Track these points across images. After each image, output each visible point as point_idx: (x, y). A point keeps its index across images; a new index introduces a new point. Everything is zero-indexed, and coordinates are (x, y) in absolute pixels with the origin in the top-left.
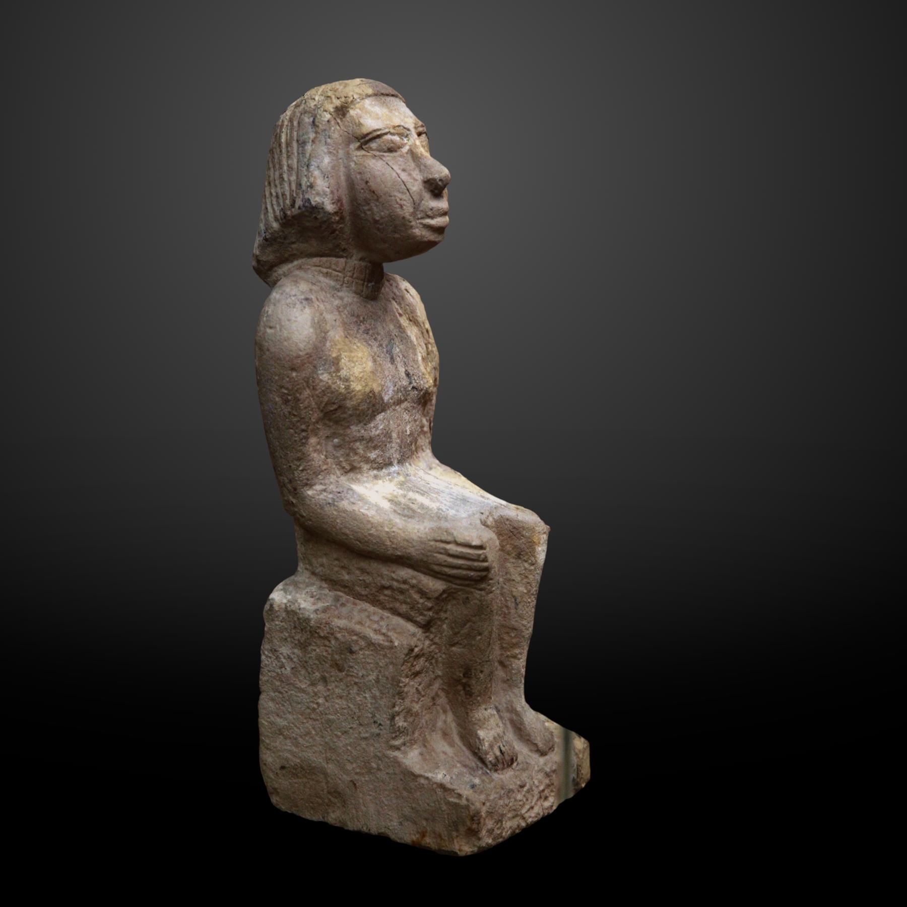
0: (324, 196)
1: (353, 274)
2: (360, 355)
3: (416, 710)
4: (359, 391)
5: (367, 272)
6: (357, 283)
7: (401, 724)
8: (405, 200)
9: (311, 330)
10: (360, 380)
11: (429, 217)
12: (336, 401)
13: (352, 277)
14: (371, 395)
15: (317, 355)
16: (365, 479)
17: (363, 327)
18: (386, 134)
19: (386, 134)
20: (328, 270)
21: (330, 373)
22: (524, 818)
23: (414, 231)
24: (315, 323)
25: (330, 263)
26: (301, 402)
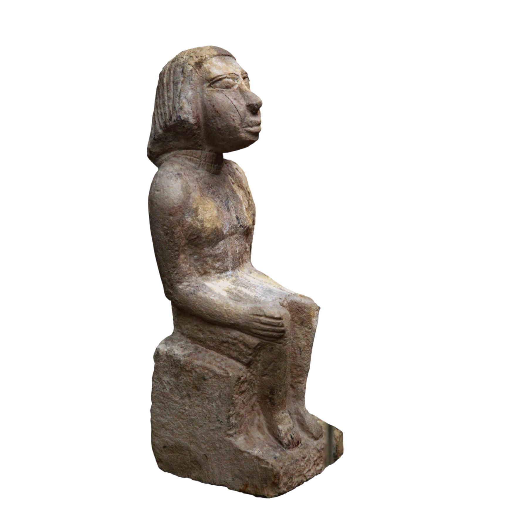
0: (189, 114)
1: (206, 159)
2: (210, 207)
3: (242, 413)
4: (209, 228)
5: (214, 158)
6: (208, 165)
7: (233, 421)
8: (236, 117)
9: (181, 192)
10: (210, 221)
11: (250, 126)
12: (196, 234)
13: (205, 161)
14: (216, 230)
15: (184, 207)
16: (213, 279)
17: (211, 190)
18: (225, 78)
19: (225, 78)
20: (191, 157)
21: (192, 217)
23: (241, 134)
24: (183, 188)
25: (192, 153)
26: (175, 234)
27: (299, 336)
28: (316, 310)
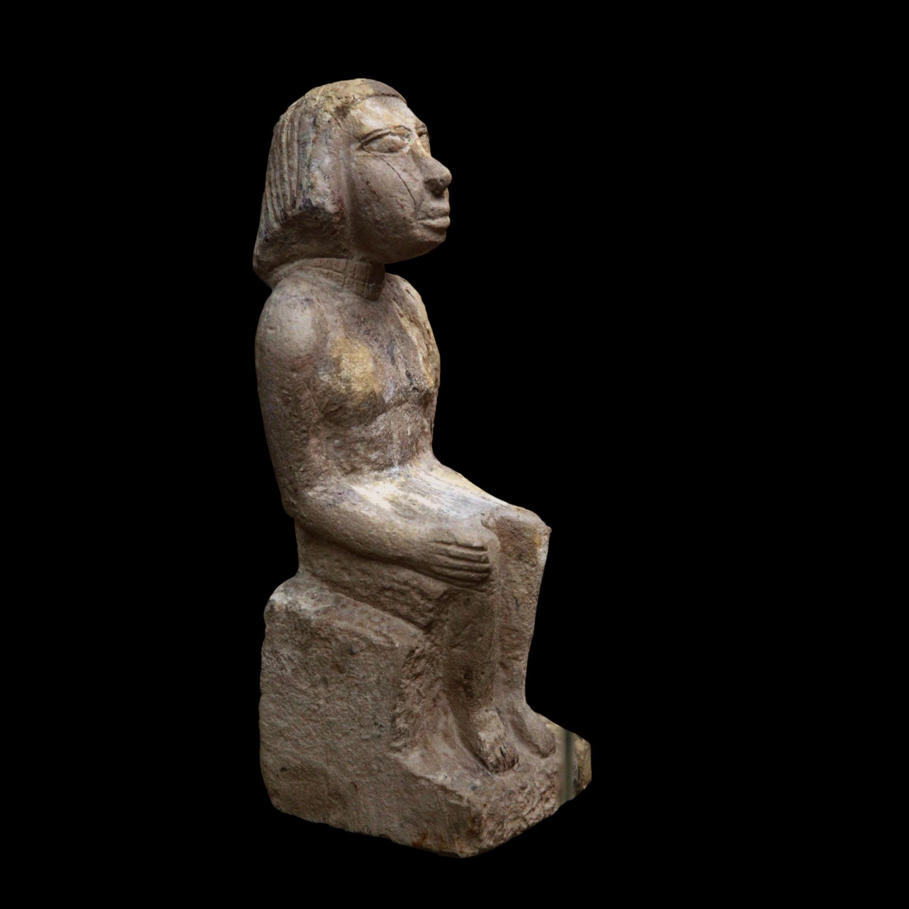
0: (325, 197)
1: (354, 274)
2: (361, 356)
3: (416, 712)
4: (360, 392)
5: (368, 272)
6: (357, 283)
8: (406, 201)
9: (312, 331)
10: (361, 381)
11: (430, 217)
12: (337, 402)
13: (352, 277)
14: (372, 396)
15: (318, 356)
16: (366, 480)
17: (363, 328)
18: (387, 134)
19: (387, 134)
20: (329, 270)
21: (331, 374)
22: (525, 820)
23: (415, 231)
24: (315, 324)
25: (331, 264)
26: (302, 403)
27: (514, 579)
28: (544, 533)
